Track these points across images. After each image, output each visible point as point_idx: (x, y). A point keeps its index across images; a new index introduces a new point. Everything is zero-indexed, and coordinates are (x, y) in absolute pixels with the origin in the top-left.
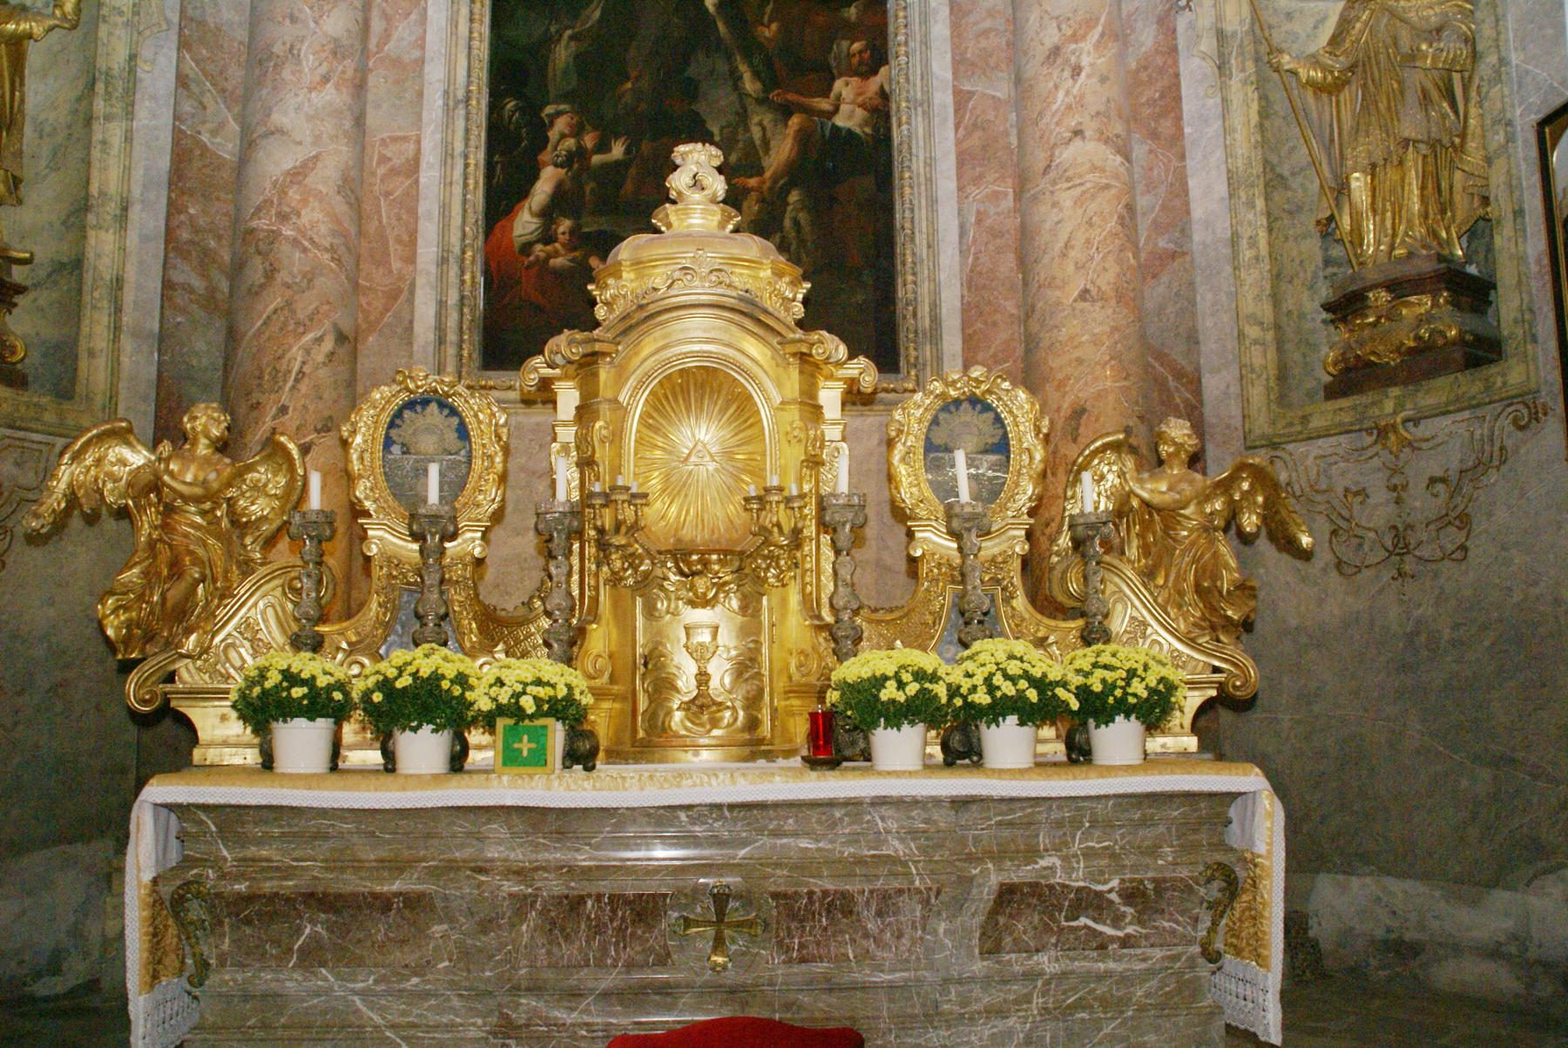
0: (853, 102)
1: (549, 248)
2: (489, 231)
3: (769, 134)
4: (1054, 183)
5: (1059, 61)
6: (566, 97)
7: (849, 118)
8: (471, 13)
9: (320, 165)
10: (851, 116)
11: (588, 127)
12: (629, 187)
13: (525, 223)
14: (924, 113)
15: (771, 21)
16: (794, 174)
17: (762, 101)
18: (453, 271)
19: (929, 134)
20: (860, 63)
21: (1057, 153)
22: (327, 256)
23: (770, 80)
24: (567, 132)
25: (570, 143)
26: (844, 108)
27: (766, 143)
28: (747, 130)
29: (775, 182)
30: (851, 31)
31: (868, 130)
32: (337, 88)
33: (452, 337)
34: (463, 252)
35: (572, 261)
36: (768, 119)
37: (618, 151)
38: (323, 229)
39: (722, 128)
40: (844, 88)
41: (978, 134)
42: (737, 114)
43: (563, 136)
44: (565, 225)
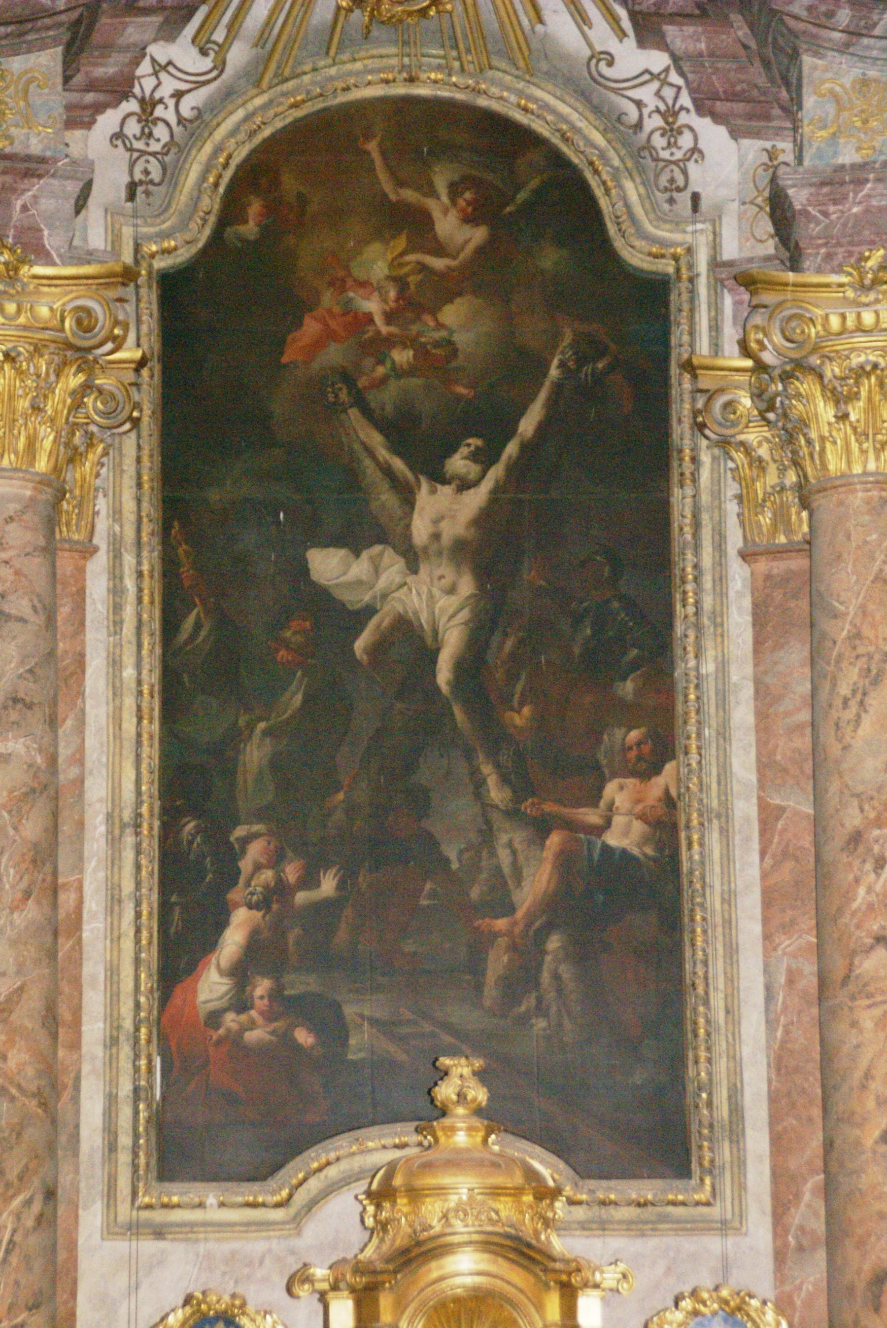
0: (629, 813)
1: (243, 1017)
2: (164, 1000)
3: (521, 858)
4: (853, 998)
5: (861, 849)
6: (261, 815)
7: (625, 835)
8: (139, 708)
9: (25, 996)
10: (626, 833)
11: (290, 854)
12: (342, 936)
13: (211, 985)
14: (721, 828)
15: (522, 704)
16: (557, 910)
17: (513, 814)
18: (126, 1050)
19: (728, 858)
20: (640, 758)
21: (856, 962)
22: (34, 1102)
23: (521, 785)
24: (263, 860)
25: (268, 875)
26: (619, 821)
27: (518, 877)
28: (493, 854)
29: (528, 926)
30: (629, 714)
31: (649, 851)
32: (39, 903)
33: (125, 1140)
34: (137, 1030)
35: (272, 1033)
36: (520, 837)
37: (328, 885)
38: (30, 1072)
39: (461, 852)
40: (618, 793)
41: (789, 865)
42: (480, 831)
43: (258, 867)
44: (262, 987)
